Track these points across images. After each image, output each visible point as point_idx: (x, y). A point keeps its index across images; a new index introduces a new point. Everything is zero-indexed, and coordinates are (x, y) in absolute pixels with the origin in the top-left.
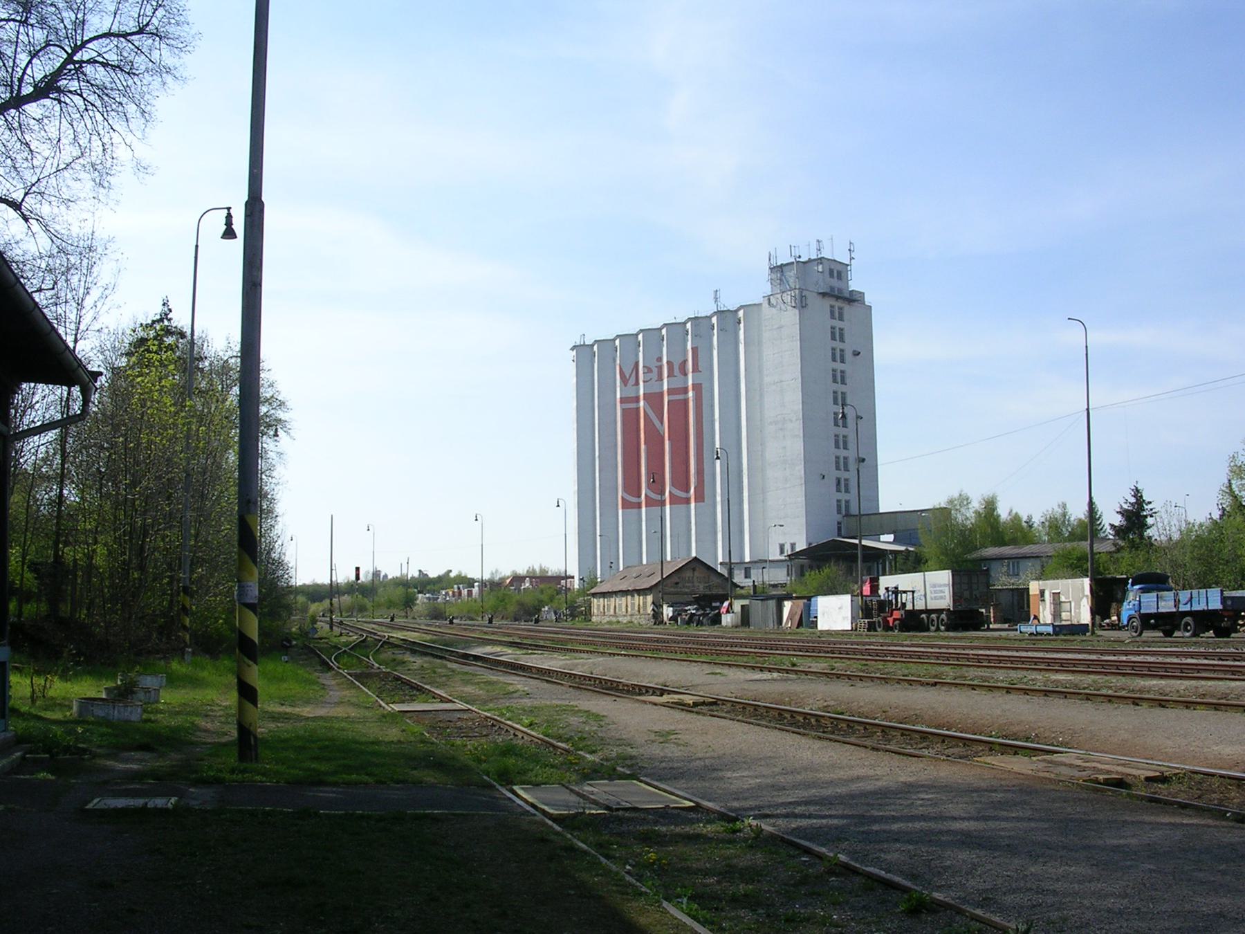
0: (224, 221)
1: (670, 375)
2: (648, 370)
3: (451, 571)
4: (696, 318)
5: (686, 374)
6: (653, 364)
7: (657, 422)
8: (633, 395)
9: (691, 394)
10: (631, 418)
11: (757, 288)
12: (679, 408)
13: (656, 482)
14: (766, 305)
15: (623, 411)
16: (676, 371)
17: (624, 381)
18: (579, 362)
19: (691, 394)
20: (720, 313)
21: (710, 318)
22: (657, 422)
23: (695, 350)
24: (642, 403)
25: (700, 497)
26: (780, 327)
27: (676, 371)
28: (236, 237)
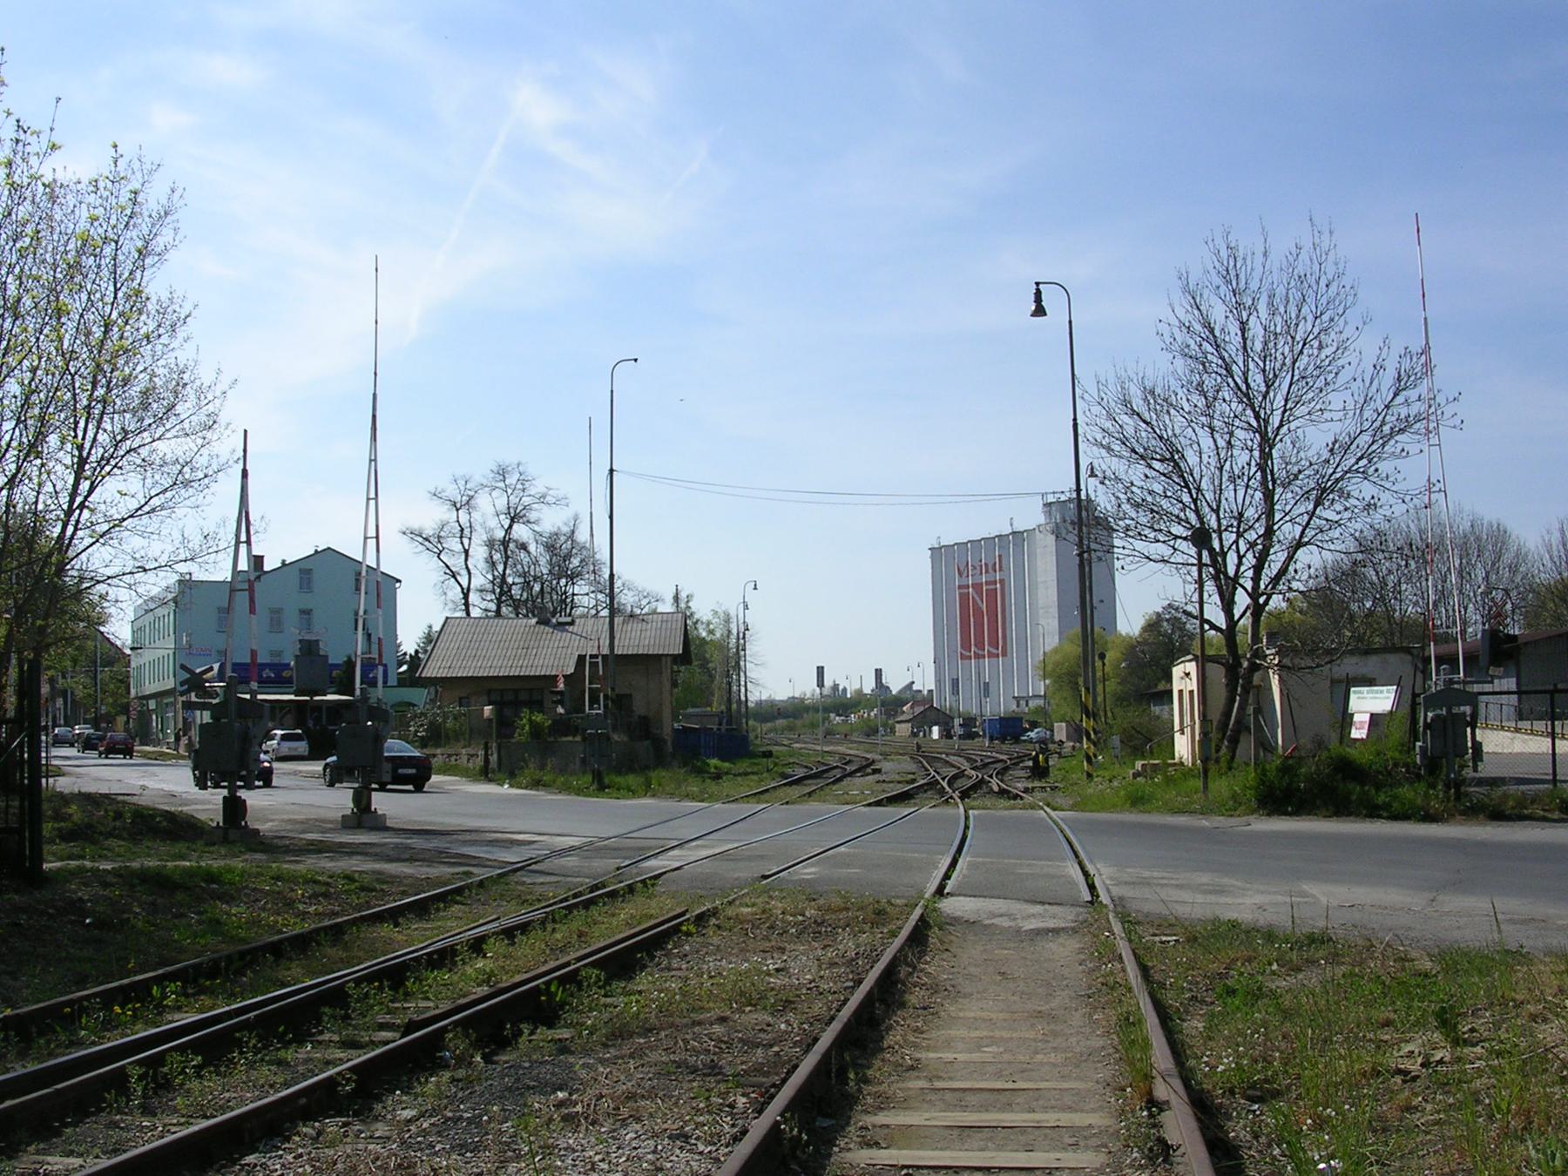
0: (1033, 298)
1: (987, 572)
2: (974, 568)
3: (913, 683)
4: (1001, 536)
5: (995, 571)
6: (977, 564)
7: (980, 602)
8: (993, 579)
9: (998, 585)
10: (964, 598)
11: (1031, 516)
12: (992, 594)
13: (980, 645)
14: (1037, 531)
15: (960, 594)
16: (990, 570)
17: (960, 574)
18: (932, 557)
19: (998, 585)
20: (1014, 533)
21: (1008, 535)
22: (980, 602)
23: (1000, 556)
24: (971, 590)
25: (1004, 654)
26: (1046, 546)
27: (990, 570)
28: (1046, 315)
